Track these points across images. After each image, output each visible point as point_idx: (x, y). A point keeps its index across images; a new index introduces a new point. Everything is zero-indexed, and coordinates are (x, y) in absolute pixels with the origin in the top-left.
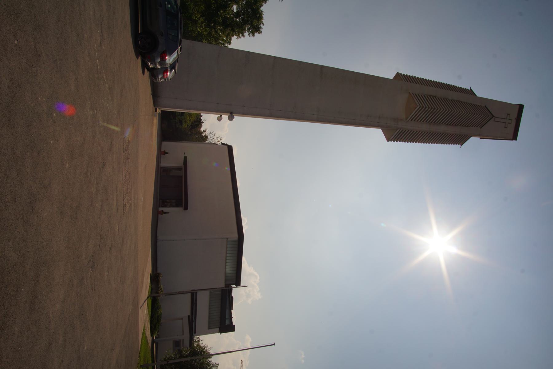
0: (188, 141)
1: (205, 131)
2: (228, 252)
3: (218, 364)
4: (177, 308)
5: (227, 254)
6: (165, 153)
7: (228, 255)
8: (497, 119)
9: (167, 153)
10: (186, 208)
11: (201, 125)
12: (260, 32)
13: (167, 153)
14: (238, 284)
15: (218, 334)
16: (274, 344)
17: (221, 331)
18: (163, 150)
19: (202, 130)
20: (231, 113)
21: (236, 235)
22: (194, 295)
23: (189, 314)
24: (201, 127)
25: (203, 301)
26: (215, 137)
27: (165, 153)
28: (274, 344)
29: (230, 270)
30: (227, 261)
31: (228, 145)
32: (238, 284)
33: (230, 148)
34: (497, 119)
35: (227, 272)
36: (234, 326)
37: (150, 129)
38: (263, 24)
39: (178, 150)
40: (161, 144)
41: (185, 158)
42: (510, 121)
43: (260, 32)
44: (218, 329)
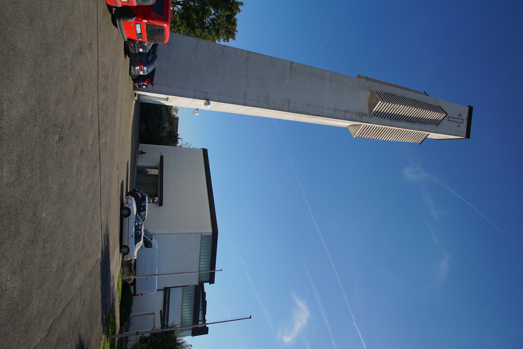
2: (202, 254)
3: (191, 346)
4: (150, 301)
6: (142, 153)
8: (450, 119)
9: (144, 153)
10: (161, 204)
12: (234, 38)
13: (144, 153)
14: (212, 281)
16: (251, 318)
18: (140, 150)
20: (207, 100)
21: (210, 230)
22: (167, 291)
23: (161, 308)
25: (176, 297)
27: (142, 153)
28: (251, 318)
29: (205, 267)
32: (212, 281)
33: (205, 151)
34: (450, 119)
38: (237, 31)
39: (152, 152)
40: (139, 145)
41: (162, 157)
42: (462, 121)
43: (234, 38)
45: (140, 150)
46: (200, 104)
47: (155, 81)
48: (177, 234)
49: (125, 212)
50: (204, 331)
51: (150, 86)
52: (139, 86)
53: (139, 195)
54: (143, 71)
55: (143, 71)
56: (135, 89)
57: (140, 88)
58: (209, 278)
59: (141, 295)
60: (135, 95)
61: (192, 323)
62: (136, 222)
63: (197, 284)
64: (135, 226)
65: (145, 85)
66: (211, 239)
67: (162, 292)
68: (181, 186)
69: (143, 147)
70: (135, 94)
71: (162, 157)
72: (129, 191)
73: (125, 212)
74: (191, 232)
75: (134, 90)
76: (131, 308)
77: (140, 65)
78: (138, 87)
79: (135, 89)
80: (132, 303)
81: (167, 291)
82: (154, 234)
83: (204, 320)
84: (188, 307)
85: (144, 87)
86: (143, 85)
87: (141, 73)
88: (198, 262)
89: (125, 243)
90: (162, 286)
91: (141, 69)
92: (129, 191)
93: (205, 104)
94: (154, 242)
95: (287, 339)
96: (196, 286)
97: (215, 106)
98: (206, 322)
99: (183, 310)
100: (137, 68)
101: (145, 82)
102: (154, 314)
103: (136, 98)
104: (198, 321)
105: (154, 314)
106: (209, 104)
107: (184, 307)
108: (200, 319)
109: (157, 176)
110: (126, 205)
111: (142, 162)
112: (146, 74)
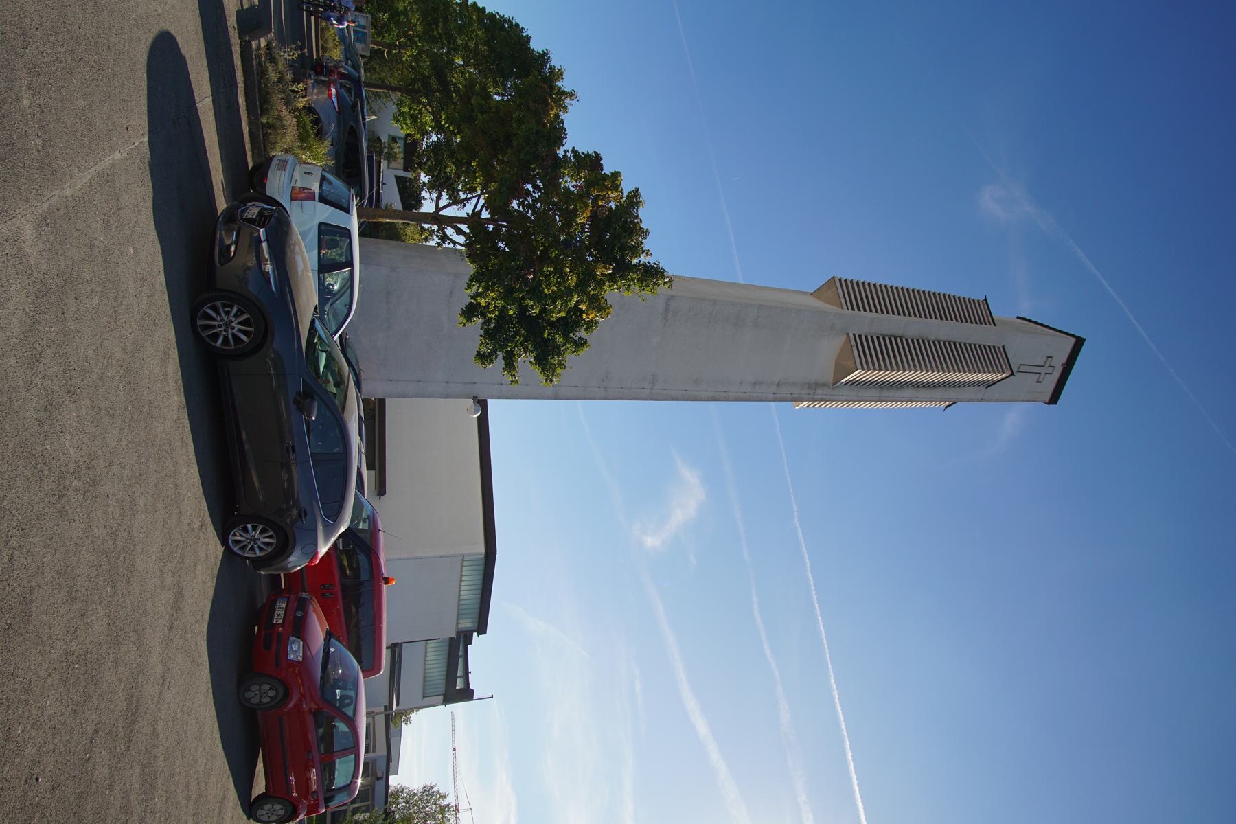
32: (482, 630)
66: (483, 562)
95: (650, 541)
108: (460, 673)
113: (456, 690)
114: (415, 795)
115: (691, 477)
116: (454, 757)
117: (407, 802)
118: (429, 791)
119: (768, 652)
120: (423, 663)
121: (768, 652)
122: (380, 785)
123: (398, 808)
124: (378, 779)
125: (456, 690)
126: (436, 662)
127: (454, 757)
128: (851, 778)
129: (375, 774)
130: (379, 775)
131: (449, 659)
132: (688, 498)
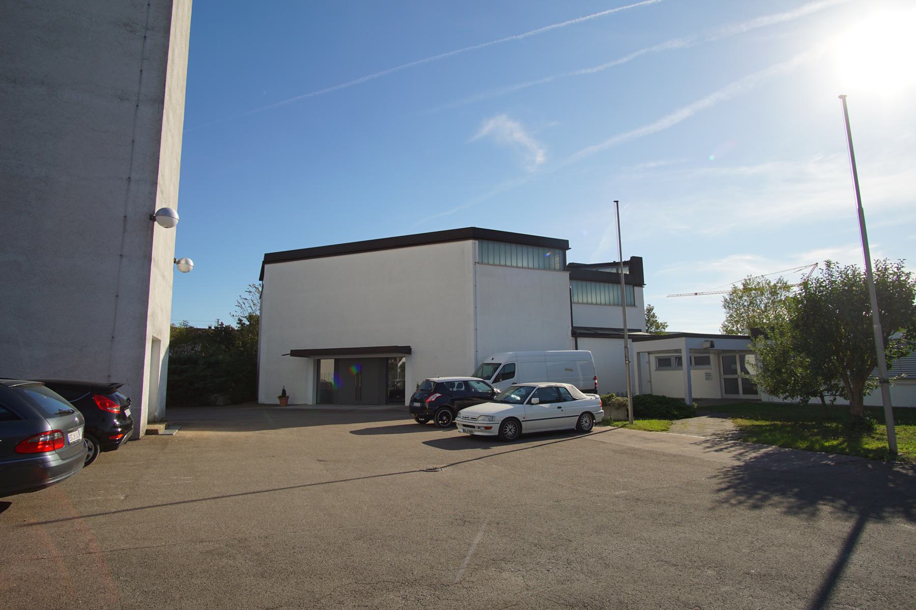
0: (256, 351)
1: (240, 320)
2: (503, 263)
5: (505, 266)
7: (509, 263)
9: (284, 391)
10: (407, 350)
11: (228, 327)
13: (284, 391)
14: (562, 246)
15: (645, 289)
17: (640, 283)
18: (278, 402)
19: (235, 326)
20: (153, 219)
22: (578, 333)
24: (233, 329)
26: (247, 295)
30: (520, 265)
31: (264, 263)
32: (562, 246)
33: (270, 259)
35: (536, 266)
36: (632, 258)
37: (216, 449)
39: (278, 374)
41: (295, 353)
44: (636, 288)
45: (278, 402)
46: (164, 240)
47: (99, 379)
48: (476, 314)
49: (510, 430)
50: (636, 264)
51: (121, 394)
52: (126, 428)
53: (432, 398)
54: (63, 432)
55: (63, 432)
56: (135, 438)
57: (131, 425)
58: (557, 251)
59: (595, 379)
60: (155, 432)
61: (619, 286)
62: (529, 403)
63: (567, 275)
64: (541, 402)
65: (123, 409)
66: (485, 243)
67: (579, 340)
68: (360, 310)
69: (267, 393)
70: (148, 432)
71: (295, 353)
72: (413, 422)
73: (511, 432)
74: (471, 284)
75: (138, 439)
76: (673, 399)
77: (37, 450)
78: (130, 433)
79: (135, 438)
80: (664, 397)
81: (578, 333)
82: (476, 359)
83: (614, 264)
84: (580, 292)
85: (128, 412)
86: (121, 416)
87: (76, 436)
88: (516, 270)
89: (572, 423)
90: (571, 340)
91: (58, 442)
92: (413, 422)
93: (168, 225)
94: (502, 359)
95: (540, 158)
96: (571, 278)
97: (168, 194)
98: (618, 260)
99: (603, 301)
100: (52, 458)
101: (110, 415)
102: (638, 353)
103: (161, 428)
104: (617, 274)
105: (638, 353)
106: (166, 212)
107: (585, 301)
108: (614, 271)
109: (337, 361)
110: (495, 431)
111: (305, 394)
112: (77, 417)
113: (631, 273)
114: (731, 316)
115: (489, 126)
116: (702, 294)
117: (737, 322)
118: (727, 304)
119: (625, 59)
120: (598, 305)
121: (625, 59)
122: (719, 345)
123: (741, 329)
124: (712, 346)
125: (631, 273)
126: (602, 295)
127: (702, 294)
128: (757, 420)
129: (706, 350)
130: (708, 345)
131: (591, 280)
132: (505, 128)
